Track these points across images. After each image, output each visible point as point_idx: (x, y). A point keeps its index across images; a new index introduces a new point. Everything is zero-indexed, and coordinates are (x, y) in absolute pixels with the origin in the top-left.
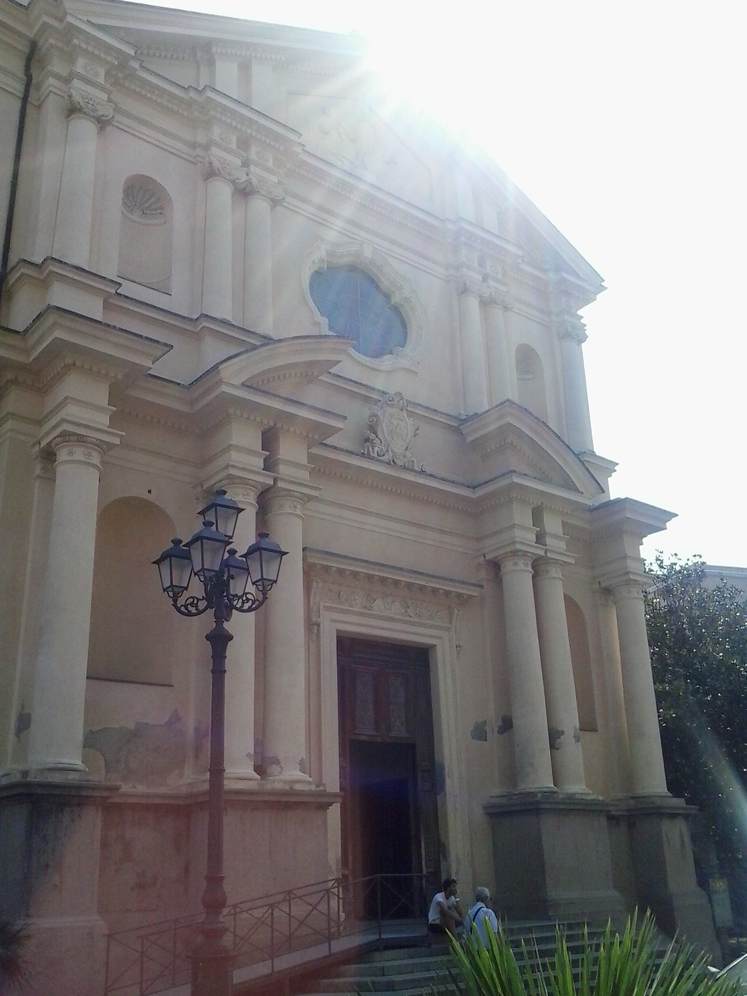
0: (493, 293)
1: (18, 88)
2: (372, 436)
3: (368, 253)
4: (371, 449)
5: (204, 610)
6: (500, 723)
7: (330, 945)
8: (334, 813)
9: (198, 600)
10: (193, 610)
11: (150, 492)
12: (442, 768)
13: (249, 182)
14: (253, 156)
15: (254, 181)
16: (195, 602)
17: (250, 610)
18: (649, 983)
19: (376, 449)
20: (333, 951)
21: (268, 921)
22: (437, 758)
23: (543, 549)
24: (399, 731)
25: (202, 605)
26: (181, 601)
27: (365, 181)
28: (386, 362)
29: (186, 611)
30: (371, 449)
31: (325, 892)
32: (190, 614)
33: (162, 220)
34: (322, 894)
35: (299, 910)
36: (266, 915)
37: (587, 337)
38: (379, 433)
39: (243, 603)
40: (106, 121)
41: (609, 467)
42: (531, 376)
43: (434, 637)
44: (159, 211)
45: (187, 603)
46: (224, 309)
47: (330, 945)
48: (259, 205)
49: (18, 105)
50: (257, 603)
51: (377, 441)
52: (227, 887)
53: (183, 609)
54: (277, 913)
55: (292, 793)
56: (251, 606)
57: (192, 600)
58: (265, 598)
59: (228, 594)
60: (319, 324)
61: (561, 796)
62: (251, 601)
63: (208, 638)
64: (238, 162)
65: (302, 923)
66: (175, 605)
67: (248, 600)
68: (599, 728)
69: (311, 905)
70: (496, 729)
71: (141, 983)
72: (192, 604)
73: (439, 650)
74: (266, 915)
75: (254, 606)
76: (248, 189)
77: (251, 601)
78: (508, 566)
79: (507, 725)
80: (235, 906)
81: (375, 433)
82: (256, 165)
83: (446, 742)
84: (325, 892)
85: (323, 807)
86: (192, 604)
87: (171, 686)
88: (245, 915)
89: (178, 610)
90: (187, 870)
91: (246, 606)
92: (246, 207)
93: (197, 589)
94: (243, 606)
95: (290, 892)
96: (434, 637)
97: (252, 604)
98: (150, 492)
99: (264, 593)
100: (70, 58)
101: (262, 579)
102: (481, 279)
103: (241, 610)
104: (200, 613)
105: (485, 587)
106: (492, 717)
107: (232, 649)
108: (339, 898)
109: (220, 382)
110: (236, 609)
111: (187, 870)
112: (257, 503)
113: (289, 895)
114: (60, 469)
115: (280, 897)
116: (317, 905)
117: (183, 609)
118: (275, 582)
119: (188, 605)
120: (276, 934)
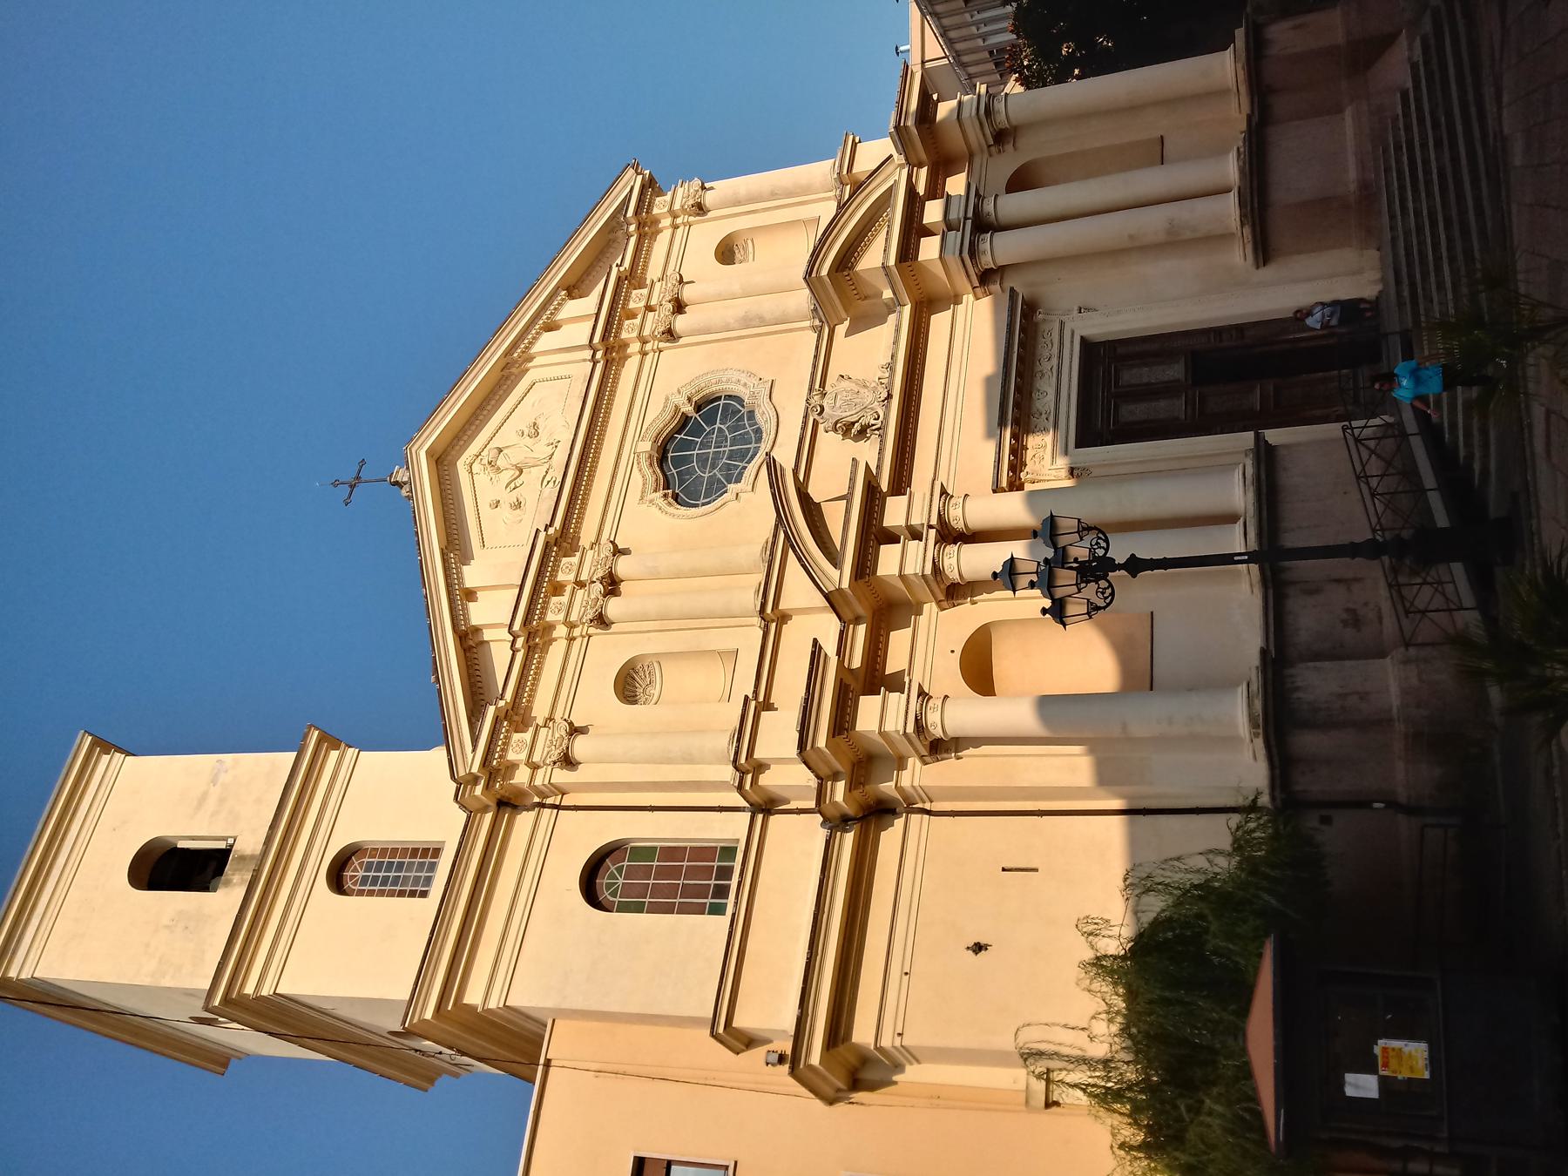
2: (857, 426)
3: (646, 446)
4: (874, 428)
5: (1108, 581)
7: (1411, 435)
8: (1273, 436)
9: (1099, 588)
10: (1109, 591)
11: (953, 651)
13: (601, 580)
15: (600, 574)
16: (1101, 590)
17: (1107, 541)
18: (1433, 279)
19: (873, 422)
20: (1416, 431)
21: (1387, 497)
23: (964, 224)
24: (1175, 371)
25: (1103, 584)
26: (1102, 604)
27: (445, 451)
30: (874, 428)
31: (1359, 444)
32: (1112, 594)
34: (1362, 449)
35: (1374, 467)
36: (1383, 499)
38: (853, 419)
39: (1100, 547)
40: (570, 728)
44: (646, 668)
47: (1411, 435)
50: (1100, 535)
51: (863, 421)
52: (1358, 540)
53: (1108, 601)
54: (1380, 490)
57: (1099, 594)
58: (1095, 528)
59: (1089, 562)
61: (1313, 322)
63: (1134, 576)
64: (580, 593)
65: (1389, 464)
66: (1104, 608)
67: (1097, 543)
69: (1370, 456)
71: (1450, 610)
72: (1103, 593)
73: (1087, 332)
74: (1383, 499)
80: (1374, 531)
84: (1359, 444)
86: (1103, 593)
87: (1152, 613)
88: (1383, 521)
89: (1108, 605)
91: (1103, 544)
93: (1090, 590)
94: (1103, 548)
95: (1358, 478)
97: (1101, 538)
98: (953, 651)
99: (1089, 529)
101: (1078, 532)
103: (1107, 550)
104: (1111, 585)
107: (1142, 554)
108: (1365, 427)
109: (839, 590)
110: (1106, 553)
111: (1338, 581)
112: (956, 544)
113: (1363, 477)
114: (951, 733)
115: (1364, 487)
116: (1376, 455)
117: (1108, 601)
118: (1079, 520)
120: (1400, 489)
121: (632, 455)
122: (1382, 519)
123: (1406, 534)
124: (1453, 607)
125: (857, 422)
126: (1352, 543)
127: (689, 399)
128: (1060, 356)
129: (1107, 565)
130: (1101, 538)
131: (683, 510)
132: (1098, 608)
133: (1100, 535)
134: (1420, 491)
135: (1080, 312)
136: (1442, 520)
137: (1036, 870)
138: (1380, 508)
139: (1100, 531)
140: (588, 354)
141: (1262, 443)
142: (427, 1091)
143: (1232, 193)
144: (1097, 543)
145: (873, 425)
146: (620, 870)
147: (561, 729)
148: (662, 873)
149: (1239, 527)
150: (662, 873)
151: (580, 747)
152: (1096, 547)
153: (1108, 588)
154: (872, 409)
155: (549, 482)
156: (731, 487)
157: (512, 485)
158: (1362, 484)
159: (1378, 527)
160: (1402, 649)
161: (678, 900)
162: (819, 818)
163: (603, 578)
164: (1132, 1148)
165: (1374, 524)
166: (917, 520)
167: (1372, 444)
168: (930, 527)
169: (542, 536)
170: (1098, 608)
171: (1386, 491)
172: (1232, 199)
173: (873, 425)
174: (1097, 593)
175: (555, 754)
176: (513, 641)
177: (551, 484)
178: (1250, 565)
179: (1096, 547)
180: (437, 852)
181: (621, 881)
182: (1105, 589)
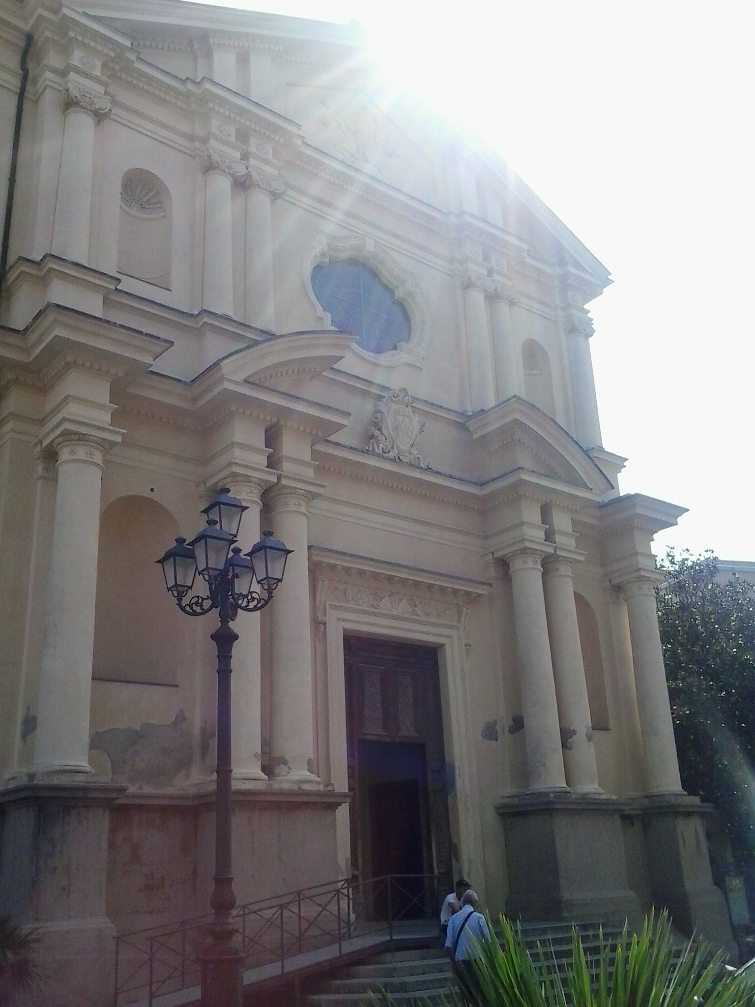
1: (14, 82)
3: (370, 246)
5: (210, 609)
6: (511, 723)
8: (343, 813)
9: (203, 599)
10: (198, 610)
11: (152, 490)
12: (453, 768)
13: (248, 175)
14: (253, 149)
16: (200, 601)
17: (255, 609)
19: (381, 446)
21: (278, 922)
22: (447, 759)
25: (207, 604)
26: (185, 601)
32: (195, 614)
33: (162, 214)
37: (594, 331)
39: (248, 602)
41: (619, 463)
45: (191, 603)
48: (259, 199)
53: (188, 608)
54: (286, 914)
62: (256, 600)
66: (179, 605)
67: (253, 599)
69: (320, 905)
72: (197, 604)
77: (256, 600)
78: (517, 565)
79: (518, 724)
80: (244, 907)
84: (334, 893)
86: (197, 604)
89: (183, 609)
91: (252, 605)
94: (248, 605)
95: (299, 893)
98: (152, 490)
99: (270, 592)
100: (66, 50)
103: (246, 609)
104: (205, 612)
106: (502, 715)
107: (238, 650)
109: (222, 379)
110: (242, 608)
113: (299, 896)
117: (188, 608)
118: (280, 580)
119: (192, 604)
120: (286, 935)
121: (363, 233)
122: (254, 914)
123: (237, 939)
124: (154, 986)
126: (231, 671)
128: (427, 623)
129: (228, 611)
132: (180, 598)
133: (263, 602)
134: (282, 953)
135: (466, 645)
136: (250, 977)
138: (267, 914)
139: (266, 603)
141: (339, 800)
143: (566, 786)
144: (253, 599)
145: (378, 446)
147: (104, 104)
149: (257, 772)
151: (82, 123)
152: (249, 597)
154: (393, 448)
158: (292, 896)
159: (247, 911)
160: (115, 934)
163: (250, 176)
165: (250, 907)
166: (287, 467)
167: (333, 908)
168: (279, 478)
170: (180, 598)
171: (284, 921)
172: (561, 783)
173: (378, 446)
174: (198, 597)
175: (74, 92)
176: (195, 82)
178: (216, 783)
182: (201, 606)
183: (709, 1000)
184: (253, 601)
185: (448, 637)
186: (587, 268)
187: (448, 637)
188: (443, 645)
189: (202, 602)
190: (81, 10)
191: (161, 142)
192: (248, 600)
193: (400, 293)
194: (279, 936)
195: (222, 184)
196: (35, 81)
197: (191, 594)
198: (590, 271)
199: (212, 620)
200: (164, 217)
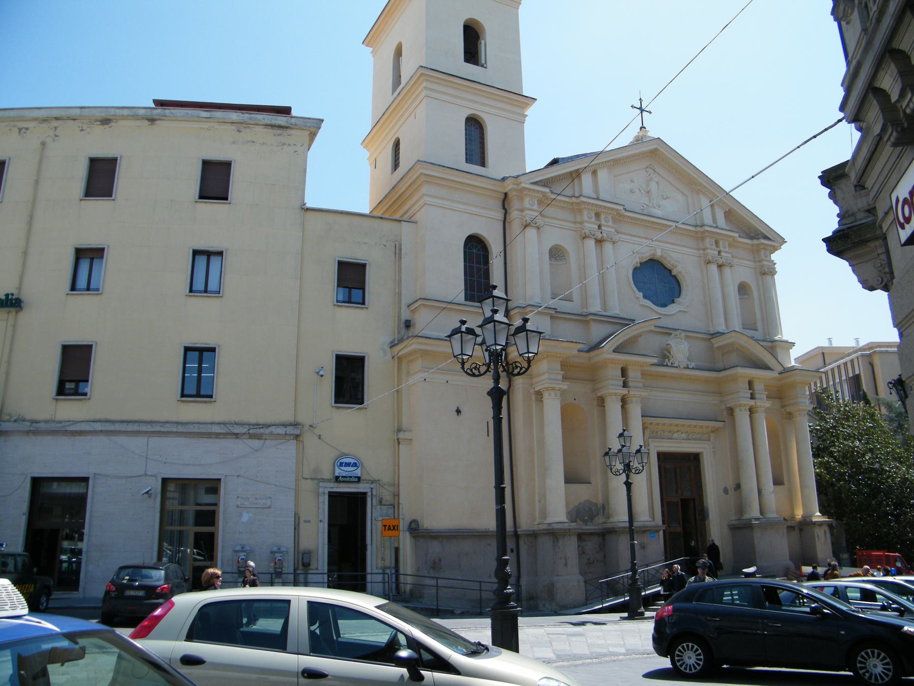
0: (724, 262)
1: (500, 216)
2: (668, 354)
3: (659, 253)
5: (485, 373)
6: (735, 486)
10: (476, 372)
11: (575, 399)
16: (478, 367)
19: (671, 361)
25: (621, 472)
28: (672, 309)
29: (471, 373)
32: (616, 475)
37: (776, 272)
41: (774, 261)
42: (747, 297)
43: (702, 448)
46: (595, 307)
49: (501, 224)
50: (523, 370)
53: (614, 473)
55: (645, 527)
56: (520, 371)
58: (529, 366)
60: (638, 298)
62: (519, 368)
67: (637, 470)
68: (785, 482)
70: (733, 489)
73: (704, 454)
75: (521, 372)
76: (602, 239)
77: (519, 368)
79: (738, 487)
81: (669, 352)
82: (605, 226)
83: (709, 496)
85: (657, 531)
87: (591, 483)
89: (466, 372)
90: (605, 557)
91: (637, 472)
92: (601, 247)
94: (513, 371)
96: (702, 448)
98: (575, 399)
100: (521, 199)
102: (717, 253)
105: (726, 421)
106: (731, 485)
111: (605, 557)
117: (469, 371)
120: (649, 575)
125: (670, 354)
127: (679, 272)
130: (521, 369)
131: (631, 272)
133: (523, 370)
137: (488, 436)
139: (527, 370)
140: (699, 223)
142: (361, 144)
146: (479, 250)
148: (479, 269)
150: (479, 269)
151: (531, 232)
153: (479, 372)
155: (643, 206)
156: (641, 294)
157: (643, 205)
161: (468, 278)
162: (620, 448)
164: (614, 531)
169: (621, 208)
177: (642, 208)
179: (514, 366)
180: (483, 164)
181: (474, 251)
182: (479, 370)
183: (641, 295)
184: (517, 368)
185: (704, 448)
186: (771, 238)
187: (704, 448)
188: (702, 453)
189: (479, 367)
190: (528, 182)
191: (560, 228)
192: (513, 367)
193: (674, 272)
194: (408, 582)
195: (591, 243)
196: (510, 214)
197: (615, 468)
198: (774, 240)
199: (487, 382)
200: (566, 263)
